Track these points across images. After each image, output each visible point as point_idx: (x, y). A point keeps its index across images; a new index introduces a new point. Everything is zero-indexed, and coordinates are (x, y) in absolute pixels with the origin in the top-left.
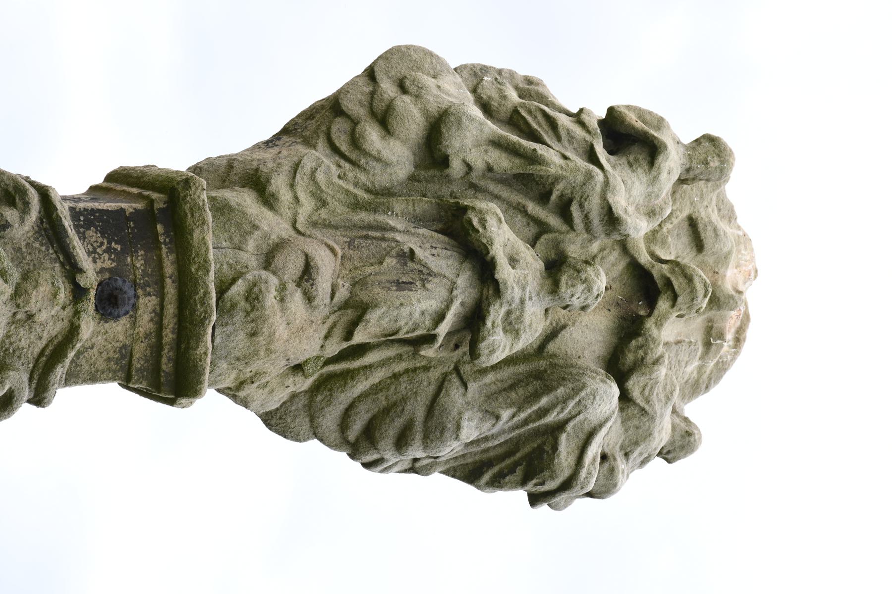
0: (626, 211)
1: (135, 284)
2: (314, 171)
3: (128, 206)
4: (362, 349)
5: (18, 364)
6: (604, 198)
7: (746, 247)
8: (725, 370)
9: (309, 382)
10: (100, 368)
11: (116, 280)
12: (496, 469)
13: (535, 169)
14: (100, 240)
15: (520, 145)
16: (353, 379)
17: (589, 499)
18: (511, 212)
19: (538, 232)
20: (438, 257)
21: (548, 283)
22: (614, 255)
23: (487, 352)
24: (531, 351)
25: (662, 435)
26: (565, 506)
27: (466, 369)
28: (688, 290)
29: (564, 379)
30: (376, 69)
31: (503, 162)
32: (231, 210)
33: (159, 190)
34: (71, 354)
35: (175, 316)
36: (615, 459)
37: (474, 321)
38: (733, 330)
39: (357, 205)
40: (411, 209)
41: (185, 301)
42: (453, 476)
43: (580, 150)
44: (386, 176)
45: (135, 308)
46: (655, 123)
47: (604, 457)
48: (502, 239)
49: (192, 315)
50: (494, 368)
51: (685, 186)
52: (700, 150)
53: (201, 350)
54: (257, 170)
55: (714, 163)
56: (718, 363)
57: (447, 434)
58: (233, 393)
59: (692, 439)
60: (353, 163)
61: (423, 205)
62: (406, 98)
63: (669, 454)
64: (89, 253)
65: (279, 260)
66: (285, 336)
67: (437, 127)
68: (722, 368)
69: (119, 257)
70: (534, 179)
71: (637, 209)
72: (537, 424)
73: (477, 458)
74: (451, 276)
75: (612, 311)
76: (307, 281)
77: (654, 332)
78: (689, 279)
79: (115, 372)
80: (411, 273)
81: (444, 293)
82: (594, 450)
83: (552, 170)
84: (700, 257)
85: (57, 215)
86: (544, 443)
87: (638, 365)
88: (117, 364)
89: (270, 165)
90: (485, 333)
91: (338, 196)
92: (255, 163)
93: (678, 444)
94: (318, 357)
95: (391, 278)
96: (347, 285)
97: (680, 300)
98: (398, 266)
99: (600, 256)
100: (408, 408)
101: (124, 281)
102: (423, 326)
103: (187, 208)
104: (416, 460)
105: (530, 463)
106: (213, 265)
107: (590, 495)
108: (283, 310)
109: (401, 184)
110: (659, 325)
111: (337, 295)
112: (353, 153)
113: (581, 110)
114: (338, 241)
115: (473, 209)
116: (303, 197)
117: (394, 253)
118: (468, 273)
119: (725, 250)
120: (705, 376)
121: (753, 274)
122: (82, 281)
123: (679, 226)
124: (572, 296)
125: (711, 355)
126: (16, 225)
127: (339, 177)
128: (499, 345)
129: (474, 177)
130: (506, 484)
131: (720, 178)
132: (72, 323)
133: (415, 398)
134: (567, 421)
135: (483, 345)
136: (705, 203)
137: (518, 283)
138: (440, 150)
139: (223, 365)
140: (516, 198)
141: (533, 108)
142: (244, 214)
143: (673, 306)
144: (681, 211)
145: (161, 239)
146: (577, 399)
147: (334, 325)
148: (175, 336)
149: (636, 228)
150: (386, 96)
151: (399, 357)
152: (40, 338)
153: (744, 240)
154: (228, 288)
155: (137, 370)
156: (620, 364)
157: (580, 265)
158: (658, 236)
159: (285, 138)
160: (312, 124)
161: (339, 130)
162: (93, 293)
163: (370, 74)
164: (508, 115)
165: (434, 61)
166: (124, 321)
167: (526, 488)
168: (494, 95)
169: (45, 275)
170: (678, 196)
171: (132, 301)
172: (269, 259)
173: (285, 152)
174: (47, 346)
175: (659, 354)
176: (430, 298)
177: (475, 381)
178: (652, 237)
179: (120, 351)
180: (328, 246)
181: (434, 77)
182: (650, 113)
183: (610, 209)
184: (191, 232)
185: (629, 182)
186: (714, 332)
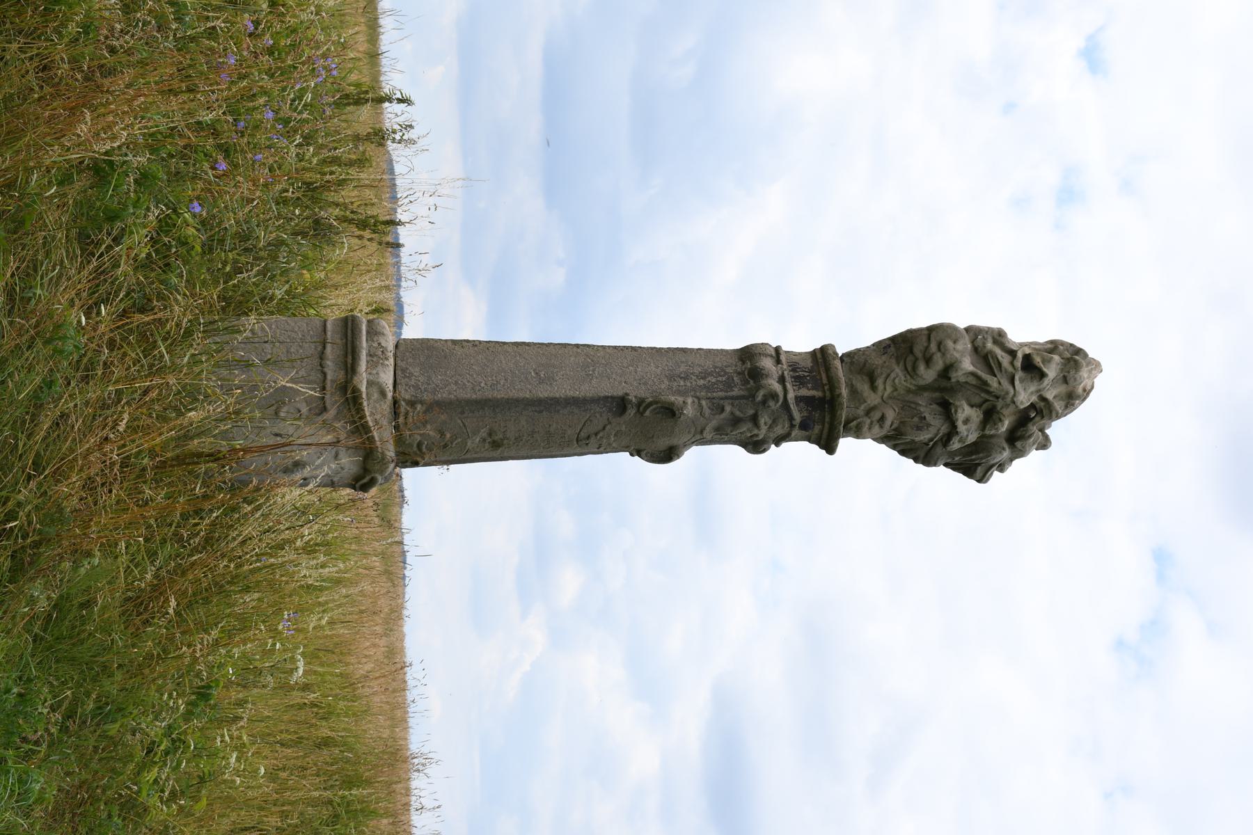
62: (939, 355)
172: (868, 413)
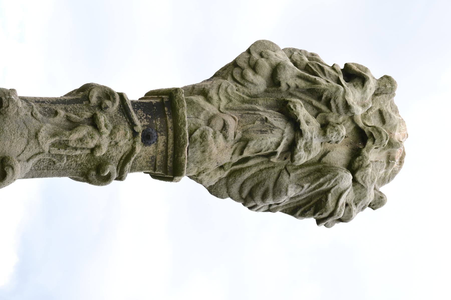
0: (353, 103)
1: (157, 131)
2: (226, 88)
3: (154, 101)
4: (247, 159)
5: (112, 163)
6: (344, 98)
7: (403, 124)
8: (396, 174)
9: (227, 173)
10: (144, 165)
11: (149, 129)
12: (302, 209)
13: (316, 86)
14: (143, 114)
15: (309, 77)
16: (244, 172)
17: (341, 224)
18: (306, 104)
19: (317, 112)
20: (278, 122)
21: (322, 132)
22: (349, 123)
23: (297, 159)
24: (316, 161)
25: (371, 197)
26: (332, 226)
27: (289, 168)
28: (380, 137)
29: (329, 171)
30: (251, 49)
31: (302, 84)
32: (194, 103)
33: (166, 95)
34: (133, 159)
35: (173, 143)
36: (351, 206)
37: (292, 148)
38: (399, 158)
39: (244, 101)
40: (266, 103)
41: (176, 137)
42: (285, 213)
43: (334, 80)
44: (255, 90)
45: (157, 140)
46: (364, 70)
47: (347, 205)
48: (303, 113)
49: (179, 143)
50: (302, 166)
51: (377, 97)
52: (383, 81)
53: (183, 157)
54: (204, 88)
55: (389, 86)
56: (392, 171)
57: (282, 193)
58: (196, 178)
59: (383, 200)
60: (242, 85)
61: (271, 101)
62: (263, 59)
63: (373, 206)
64: (139, 119)
65: (213, 122)
66: (216, 153)
67: (275, 70)
68: (394, 173)
69: (150, 120)
70: (315, 91)
71: (358, 104)
72: (319, 190)
73: (295, 205)
74: (282, 128)
75: (349, 146)
76: (224, 130)
77: (366, 154)
78: (380, 133)
79: (150, 167)
80: (266, 127)
81: (280, 135)
82: (343, 201)
83: (323, 86)
84: (384, 126)
85: (126, 103)
86: (322, 198)
87: (360, 167)
88: (150, 163)
89: (209, 86)
90: (297, 151)
91: (236, 98)
92: (203, 86)
93: (377, 202)
94: (230, 163)
95: (258, 129)
96: (240, 132)
97: (376, 141)
98: (261, 124)
99: (343, 123)
100: (266, 183)
101: (152, 130)
102: (271, 148)
103: (176, 100)
104: (270, 205)
105: (316, 206)
106: (187, 124)
107: (340, 220)
108: (215, 142)
109: (262, 93)
110: (368, 151)
111: (237, 136)
112: (242, 81)
113: (334, 65)
114: (236, 115)
115: (291, 101)
116: (222, 98)
117: (259, 119)
118: (289, 127)
119: (394, 124)
120: (388, 176)
121: (406, 136)
122: (136, 129)
123: (375, 113)
124: (332, 136)
125: (390, 167)
126: (111, 107)
127: (237, 90)
128: (302, 157)
129: (291, 90)
130: (307, 215)
131: (391, 93)
132: (132, 146)
133: (269, 179)
134: (331, 189)
135: (296, 156)
136: (386, 105)
137: (310, 131)
138: (277, 79)
139: (192, 165)
140: (308, 99)
141: (314, 64)
142: (199, 104)
143: (373, 144)
144: (376, 107)
145: (167, 113)
146: (335, 179)
147: (236, 149)
148: (173, 152)
149: (357, 110)
150: (255, 59)
151: (262, 163)
152: (121, 152)
153: (402, 121)
154: (193, 133)
155: (158, 166)
156: (354, 164)
157: (335, 125)
158: (367, 116)
159: (215, 78)
160: (225, 72)
161: (236, 73)
162: (140, 134)
163: (249, 51)
164: (304, 67)
165: (274, 46)
166: (153, 146)
167: (315, 217)
168: (298, 59)
169: (122, 127)
170: (374, 101)
171: (156, 138)
173: (215, 82)
174: (123, 155)
175: (368, 163)
176: (274, 137)
177: (293, 173)
178: (364, 116)
179: (151, 158)
180: (233, 117)
181: (274, 52)
182: (362, 66)
183: (346, 102)
184: (178, 110)
185: (354, 92)
186: (391, 158)
